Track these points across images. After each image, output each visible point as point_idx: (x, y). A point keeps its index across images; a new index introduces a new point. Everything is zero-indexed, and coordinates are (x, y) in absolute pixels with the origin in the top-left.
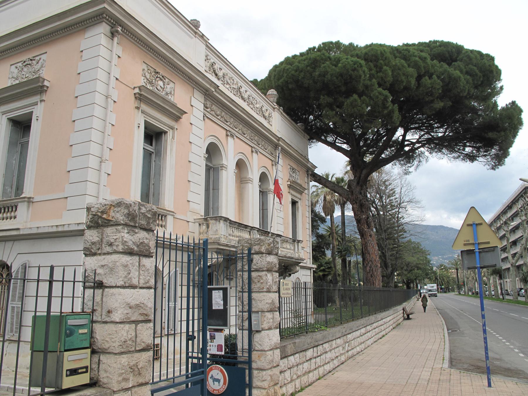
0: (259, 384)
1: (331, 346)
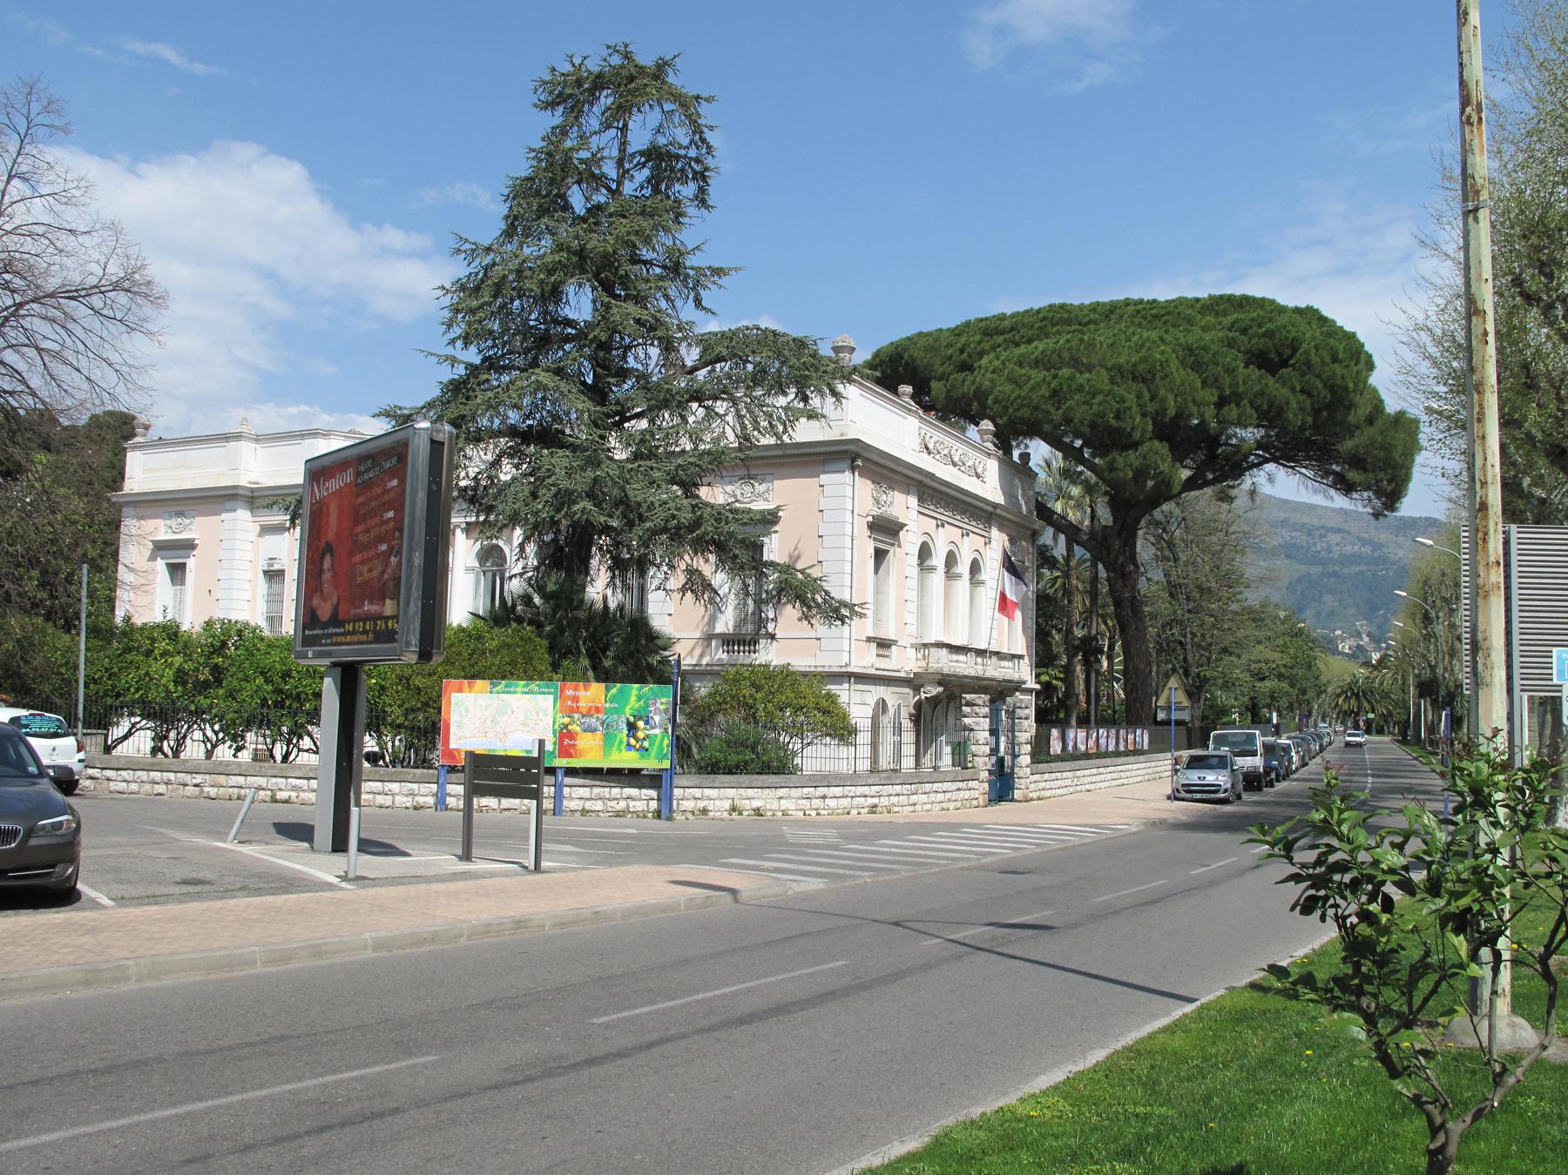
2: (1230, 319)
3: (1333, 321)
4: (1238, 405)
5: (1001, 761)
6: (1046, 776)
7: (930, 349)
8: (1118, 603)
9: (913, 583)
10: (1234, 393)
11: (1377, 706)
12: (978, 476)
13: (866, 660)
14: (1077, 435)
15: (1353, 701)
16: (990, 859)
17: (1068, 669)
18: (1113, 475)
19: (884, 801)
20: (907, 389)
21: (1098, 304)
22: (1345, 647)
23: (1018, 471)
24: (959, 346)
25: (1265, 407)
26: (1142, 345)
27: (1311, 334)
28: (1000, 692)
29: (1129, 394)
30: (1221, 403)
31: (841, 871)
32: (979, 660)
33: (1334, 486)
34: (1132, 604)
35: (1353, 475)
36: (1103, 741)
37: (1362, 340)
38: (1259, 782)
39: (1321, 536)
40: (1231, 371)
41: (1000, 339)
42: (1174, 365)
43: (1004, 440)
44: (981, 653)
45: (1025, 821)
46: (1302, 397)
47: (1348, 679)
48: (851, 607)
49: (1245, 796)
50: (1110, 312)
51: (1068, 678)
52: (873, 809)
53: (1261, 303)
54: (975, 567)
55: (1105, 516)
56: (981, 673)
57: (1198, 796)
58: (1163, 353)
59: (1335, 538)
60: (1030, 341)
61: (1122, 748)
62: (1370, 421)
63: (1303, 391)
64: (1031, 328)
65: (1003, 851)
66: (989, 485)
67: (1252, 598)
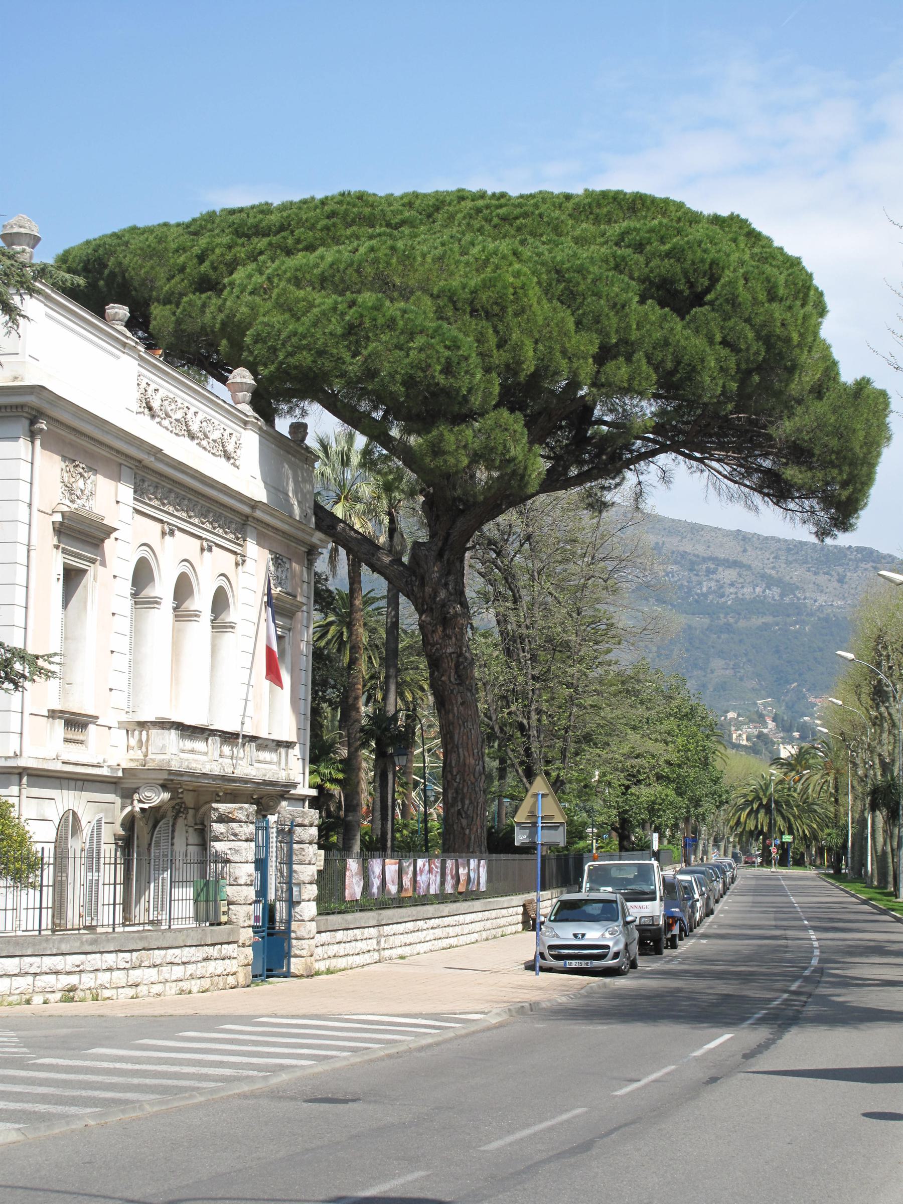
0: (298, 952)
1: (363, 934)
2: (615, 229)
3: (769, 239)
4: (629, 359)
5: (270, 912)
6: (340, 935)
7: (149, 253)
8: (435, 664)
9: (123, 624)
10: (624, 341)
11: (797, 824)
12: (228, 457)
13: (47, 747)
14: (378, 399)
15: (761, 815)
16: (284, 1077)
17: (349, 766)
18: (439, 461)
19: (88, 981)
20: (120, 311)
21: (416, 195)
22: (741, 736)
23: (291, 451)
24: (196, 250)
25: (669, 365)
26: (486, 262)
27: (737, 255)
28: (265, 797)
29: (465, 334)
30: (604, 355)
31: (41, 1108)
32: (226, 749)
33: (759, 489)
34: (457, 666)
35: (791, 473)
36: (422, 879)
37: (809, 269)
38: (657, 941)
39: (709, 572)
40: (619, 307)
41: (261, 243)
42: (534, 292)
43: (264, 404)
44: (229, 737)
45: (322, 1011)
46: (724, 352)
47: (754, 784)
48: (31, 660)
49: (642, 962)
50: (433, 209)
51: (349, 784)
52: (69, 995)
53: (663, 206)
54: (220, 602)
55: (413, 528)
56: (228, 770)
57: (574, 964)
58: (517, 274)
59: (728, 575)
60: (311, 248)
61: (449, 889)
62: (818, 391)
63: (725, 343)
64: (312, 228)
65: (302, 1065)
66: (242, 468)
67: (623, 658)
